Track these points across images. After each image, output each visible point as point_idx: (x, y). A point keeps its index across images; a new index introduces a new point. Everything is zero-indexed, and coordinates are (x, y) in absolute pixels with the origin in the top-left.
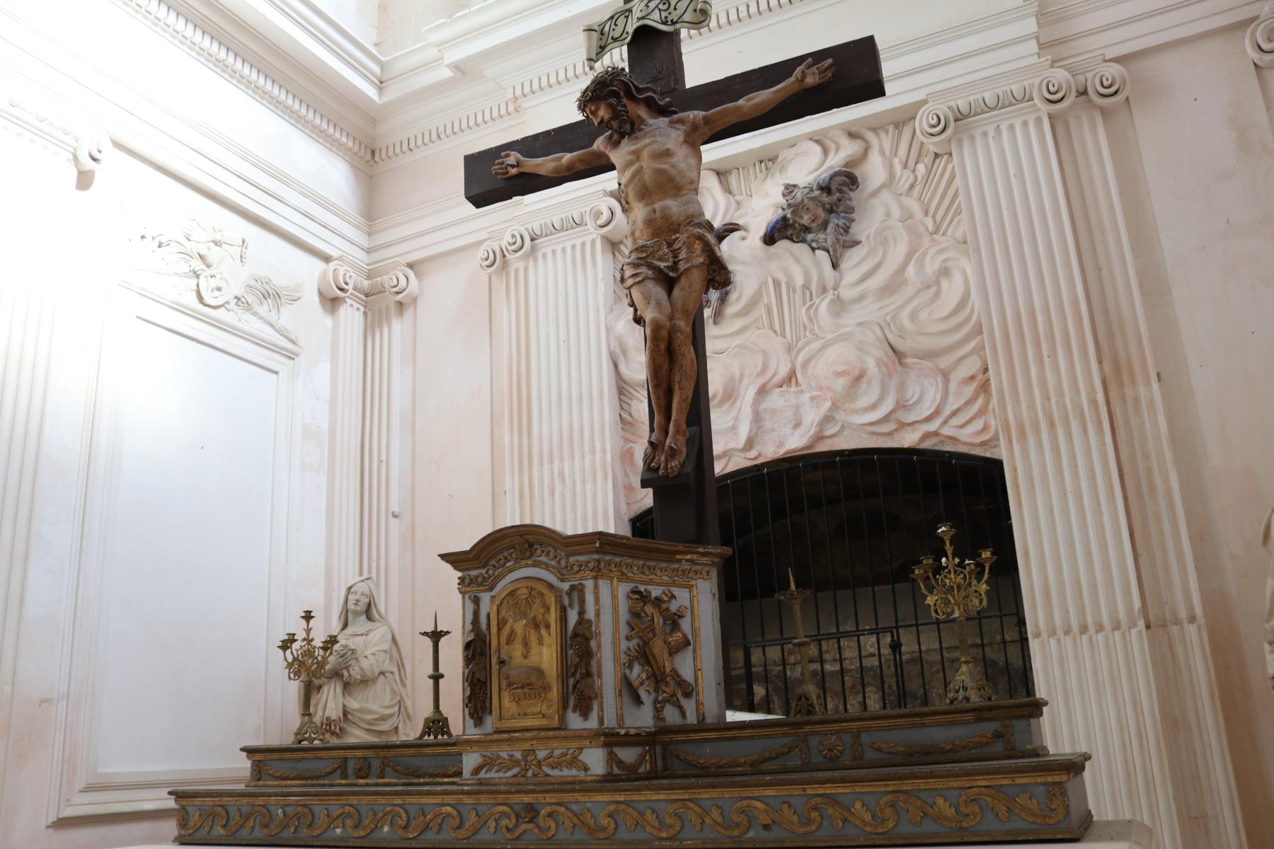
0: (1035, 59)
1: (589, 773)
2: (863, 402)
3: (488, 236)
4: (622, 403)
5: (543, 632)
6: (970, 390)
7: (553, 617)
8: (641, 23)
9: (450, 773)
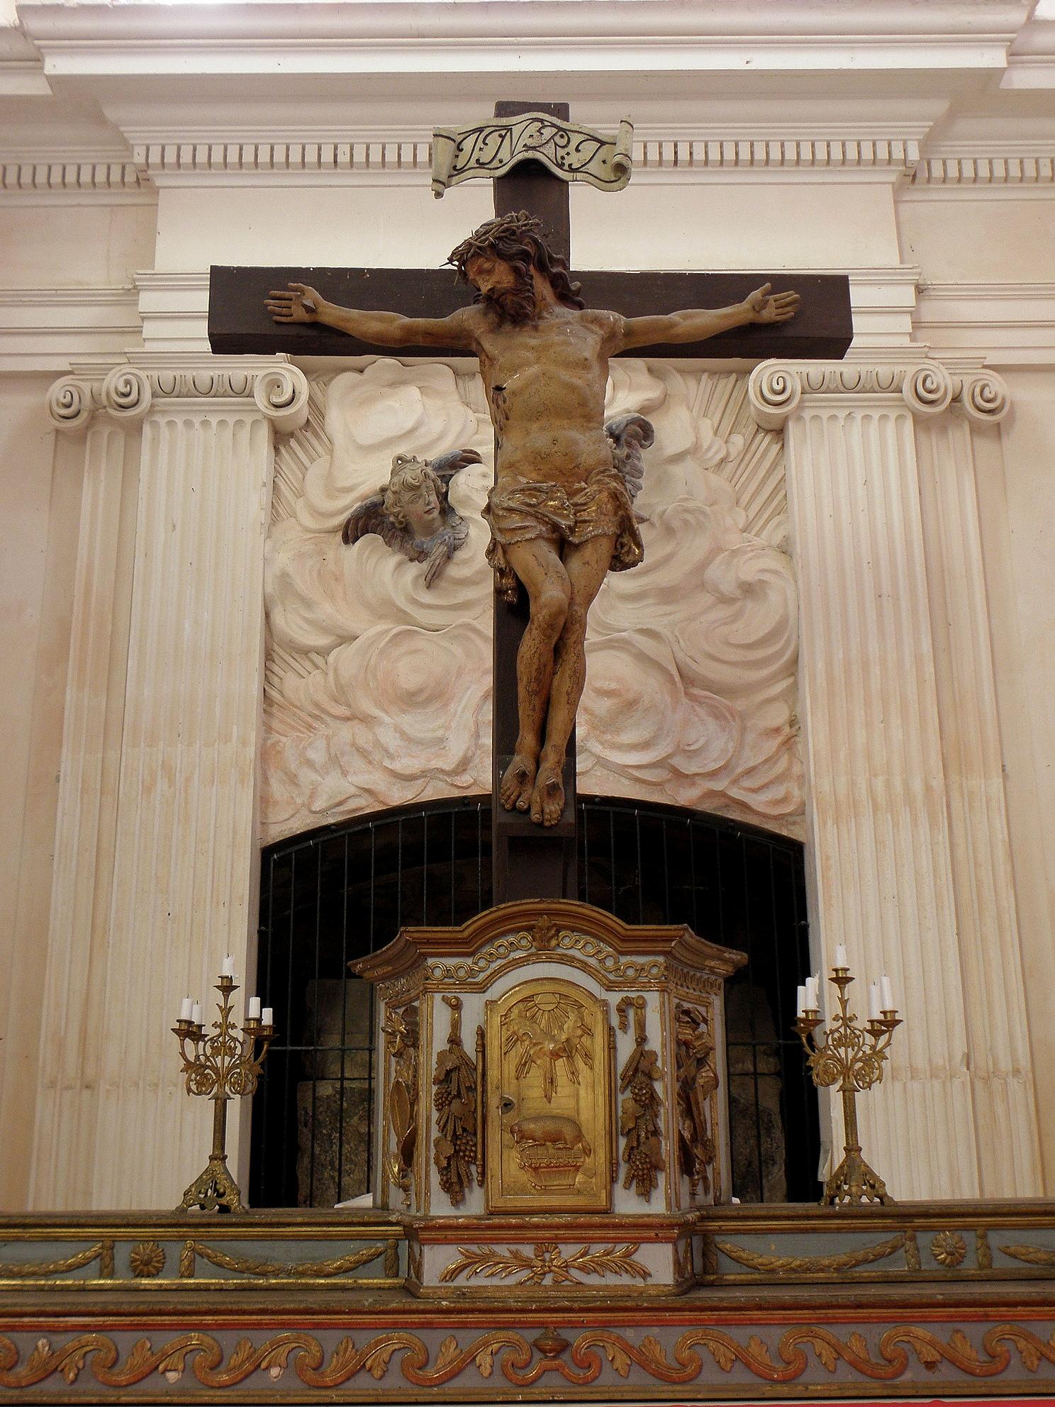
0: (906, 341)
1: (650, 1281)
2: (628, 737)
3: (68, 368)
4: (267, 672)
5: (580, 1064)
6: (772, 745)
7: (598, 1044)
8: (530, 155)
9: (330, 1269)
